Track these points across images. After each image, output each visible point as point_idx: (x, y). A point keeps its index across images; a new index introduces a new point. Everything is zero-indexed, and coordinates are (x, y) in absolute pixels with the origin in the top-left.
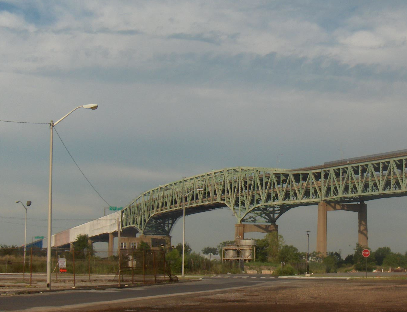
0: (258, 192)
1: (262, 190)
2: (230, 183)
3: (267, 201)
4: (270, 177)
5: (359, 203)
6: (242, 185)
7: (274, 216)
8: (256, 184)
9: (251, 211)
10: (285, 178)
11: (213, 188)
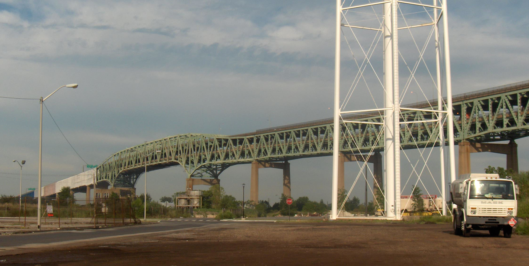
0: (204, 153)
1: (207, 152)
3: (211, 160)
4: (214, 142)
5: (284, 162)
7: (216, 172)
9: (199, 168)
10: (226, 143)
11: (169, 150)
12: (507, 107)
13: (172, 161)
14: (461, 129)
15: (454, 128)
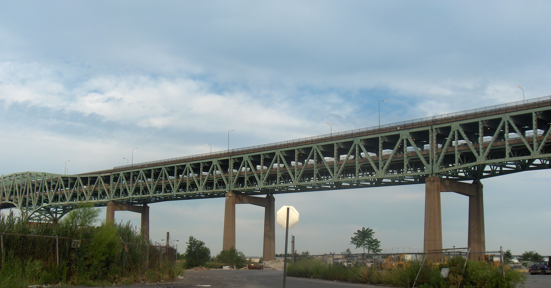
0: (16, 197)
1: (20, 195)
2: (18, 186)
3: (72, 200)
4: (58, 181)
5: (142, 205)
6: (30, 187)
7: (56, 216)
8: (43, 186)
9: (37, 210)
10: (73, 182)
11: (2, 190)
12: (143, 179)
13: (5, 202)
14: (228, 181)
15: (378, 165)
